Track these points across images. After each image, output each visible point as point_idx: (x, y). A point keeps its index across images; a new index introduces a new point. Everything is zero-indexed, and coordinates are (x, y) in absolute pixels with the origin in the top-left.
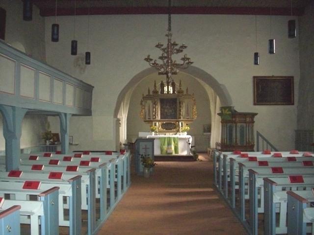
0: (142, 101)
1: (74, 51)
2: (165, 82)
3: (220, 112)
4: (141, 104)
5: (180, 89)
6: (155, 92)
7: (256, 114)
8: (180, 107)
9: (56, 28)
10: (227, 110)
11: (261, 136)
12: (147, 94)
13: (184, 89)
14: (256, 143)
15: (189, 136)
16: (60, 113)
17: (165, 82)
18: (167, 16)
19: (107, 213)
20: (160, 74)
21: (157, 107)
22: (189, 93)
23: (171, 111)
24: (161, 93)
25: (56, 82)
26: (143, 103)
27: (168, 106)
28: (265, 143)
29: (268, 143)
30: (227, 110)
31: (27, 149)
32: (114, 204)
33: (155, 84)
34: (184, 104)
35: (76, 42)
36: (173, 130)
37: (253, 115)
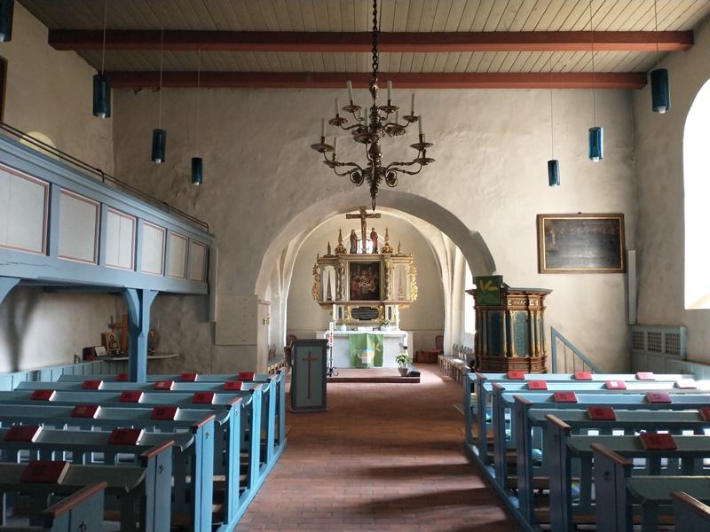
1: (158, 149)
2: (358, 232)
3: (475, 287)
4: (315, 272)
5: (387, 244)
6: (340, 250)
7: (547, 292)
10: (490, 282)
11: (560, 337)
13: (393, 244)
15: (404, 332)
16: (124, 290)
17: (358, 232)
19: (260, 475)
20: (349, 217)
21: (343, 278)
23: (369, 285)
24: (351, 252)
25: (65, 206)
26: (319, 270)
28: (569, 352)
30: (490, 282)
31: (51, 368)
32: (237, 508)
33: (340, 235)
34: (393, 272)
37: (542, 294)
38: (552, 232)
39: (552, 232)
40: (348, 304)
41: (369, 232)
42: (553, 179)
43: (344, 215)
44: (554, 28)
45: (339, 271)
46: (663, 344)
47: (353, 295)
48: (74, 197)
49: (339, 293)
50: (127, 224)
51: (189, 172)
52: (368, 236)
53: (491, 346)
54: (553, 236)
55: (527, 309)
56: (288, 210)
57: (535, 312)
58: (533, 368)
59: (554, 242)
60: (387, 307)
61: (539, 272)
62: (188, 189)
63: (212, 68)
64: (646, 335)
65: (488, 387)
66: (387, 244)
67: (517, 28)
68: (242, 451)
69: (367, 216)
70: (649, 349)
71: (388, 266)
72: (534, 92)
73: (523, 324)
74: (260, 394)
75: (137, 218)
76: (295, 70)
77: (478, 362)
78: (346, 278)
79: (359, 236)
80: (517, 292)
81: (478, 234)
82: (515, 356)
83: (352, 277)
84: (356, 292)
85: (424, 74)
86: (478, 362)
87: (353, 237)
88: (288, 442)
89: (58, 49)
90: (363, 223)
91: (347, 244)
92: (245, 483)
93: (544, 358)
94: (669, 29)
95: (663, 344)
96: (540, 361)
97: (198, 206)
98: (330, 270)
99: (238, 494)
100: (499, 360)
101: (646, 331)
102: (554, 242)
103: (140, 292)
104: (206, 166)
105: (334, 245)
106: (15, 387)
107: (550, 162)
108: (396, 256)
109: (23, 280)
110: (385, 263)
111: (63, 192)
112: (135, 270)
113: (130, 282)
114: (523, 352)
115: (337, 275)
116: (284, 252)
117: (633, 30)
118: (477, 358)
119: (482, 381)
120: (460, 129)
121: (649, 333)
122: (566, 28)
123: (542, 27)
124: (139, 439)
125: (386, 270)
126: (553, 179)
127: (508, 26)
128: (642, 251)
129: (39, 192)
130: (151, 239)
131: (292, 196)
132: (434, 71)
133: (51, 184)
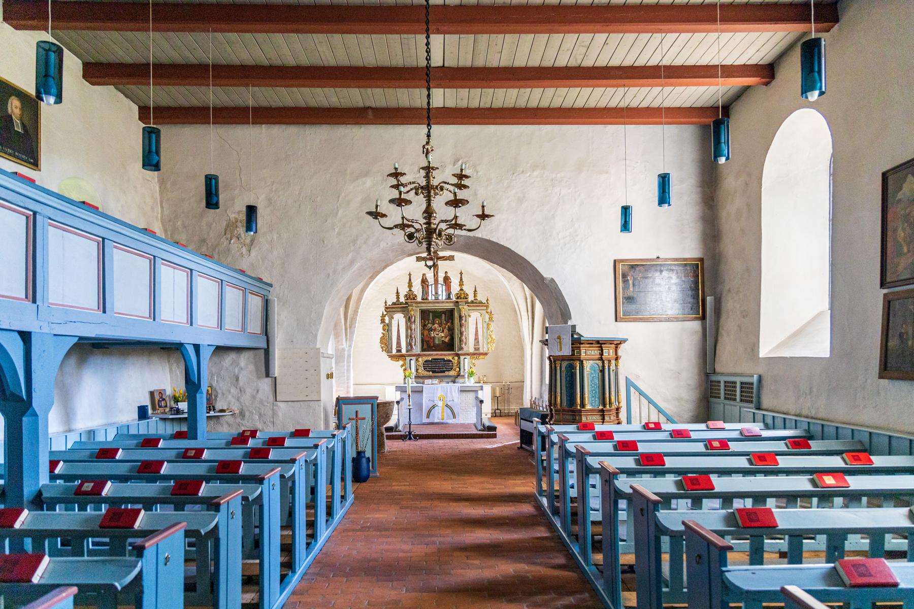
0: (383, 316)
1: (211, 200)
4: (383, 321)
5: (461, 290)
6: (410, 296)
7: (625, 341)
8: (461, 326)
9: (154, 136)
12: (395, 300)
13: (468, 290)
14: (623, 404)
16: (181, 345)
18: (424, 129)
22: (479, 298)
23: (443, 335)
26: (387, 319)
27: (436, 325)
28: (645, 402)
29: (650, 402)
33: (410, 280)
35: (216, 178)
36: (447, 373)
37: (617, 344)
38: (629, 275)
39: (629, 275)
40: (419, 355)
41: (441, 276)
42: (626, 226)
43: (414, 257)
44: (628, 62)
45: (409, 320)
46: (722, 392)
47: (425, 347)
48: (128, 252)
49: (410, 345)
50: (181, 277)
51: (243, 217)
52: (441, 280)
53: (565, 398)
54: (631, 282)
55: (601, 359)
56: (350, 256)
57: (610, 361)
58: (607, 418)
59: (631, 289)
60: (462, 358)
61: (616, 320)
62: (243, 236)
63: (265, 104)
64: (722, 384)
65: (555, 438)
66: (461, 290)
67: (588, 63)
68: (308, 507)
69: (439, 258)
70: (725, 398)
71: (463, 314)
72: (611, 128)
73: (597, 375)
74: (324, 448)
75: (191, 270)
76: (355, 105)
77: (552, 414)
78: (417, 327)
79: (431, 280)
80: (590, 343)
81: (553, 280)
82: (588, 407)
83: (424, 326)
84: (428, 342)
85: (494, 109)
86: (552, 414)
87: (424, 281)
88: (356, 498)
89: (93, 84)
90: (435, 266)
91: (417, 290)
92: (312, 537)
93: (618, 409)
94: (749, 63)
95: (722, 392)
96: (614, 412)
97: (253, 252)
98: (399, 319)
99: (305, 546)
100: (573, 411)
101: (722, 379)
102: (631, 289)
103: (197, 347)
104: (261, 212)
105: (404, 291)
106: (69, 447)
107: (623, 207)
108: (472, 302)
109: (81, 338)
110: (460, 310)
111: (116, 247)
112: (191, 325)
113: (186, 337)
114: (597, 403)
115: (406, 323)
116: (349, 299)
117: (711, 64)
118: (551, 410)
119: (550, 431)
120: (534, 168)
121: (742, 383)
122: (641, 62)
123: (615, 62)
124: (201, 491)
125: (461, 317)
126: (626, 226)
127: (579, 62)
128: (720, 298)
129: (92, 248)
130: (206, 290)
131: (354, 242)
132: (505, 106)
133: (104, 239)
